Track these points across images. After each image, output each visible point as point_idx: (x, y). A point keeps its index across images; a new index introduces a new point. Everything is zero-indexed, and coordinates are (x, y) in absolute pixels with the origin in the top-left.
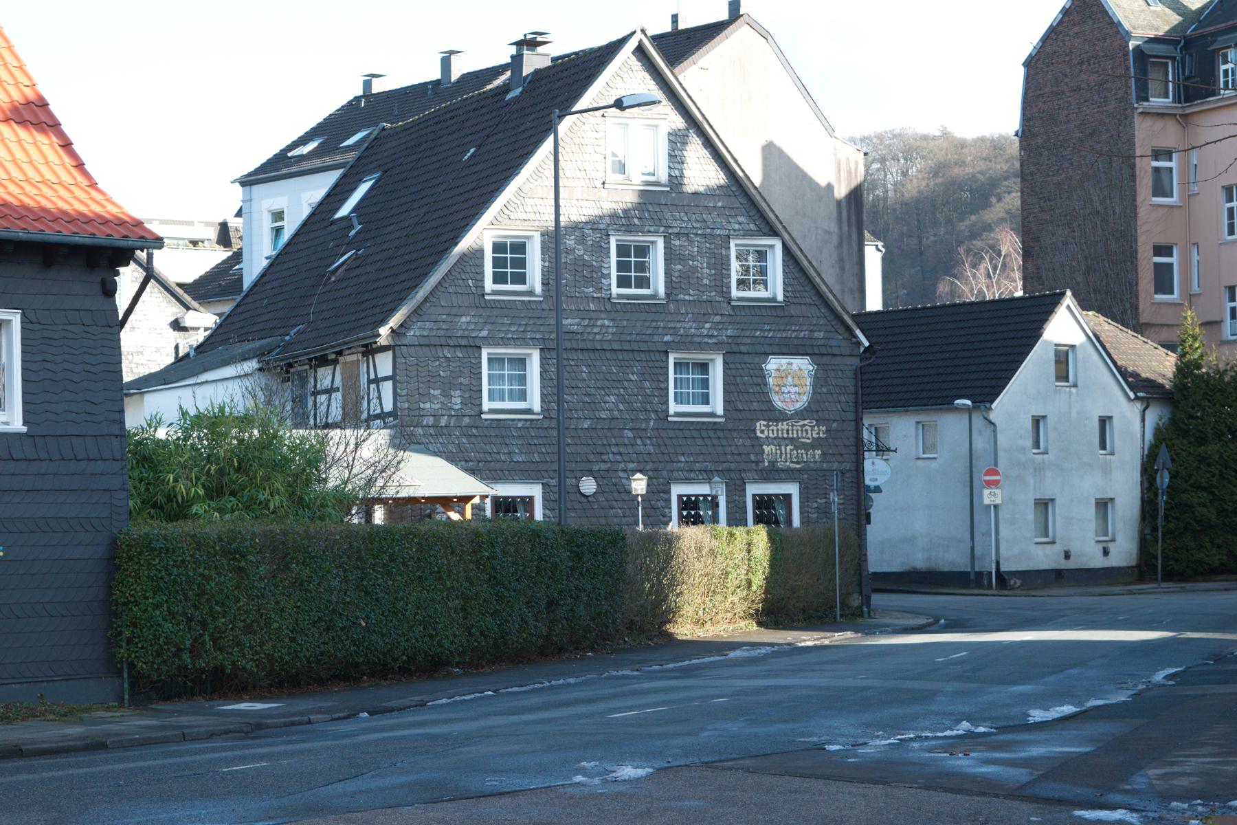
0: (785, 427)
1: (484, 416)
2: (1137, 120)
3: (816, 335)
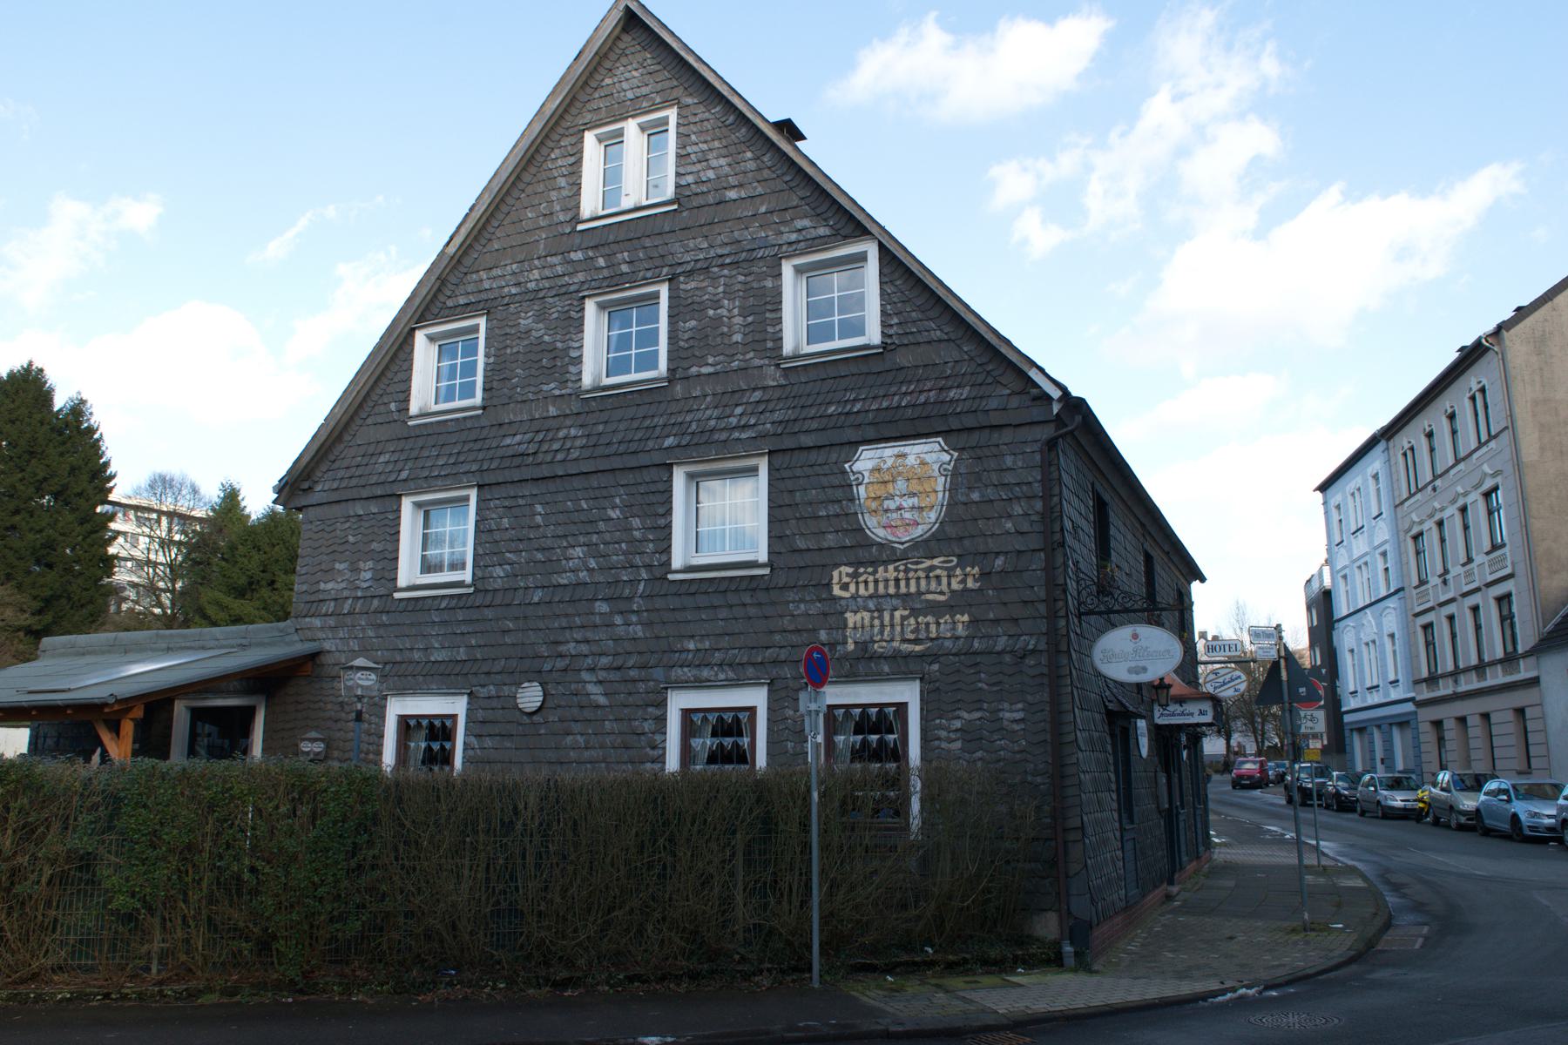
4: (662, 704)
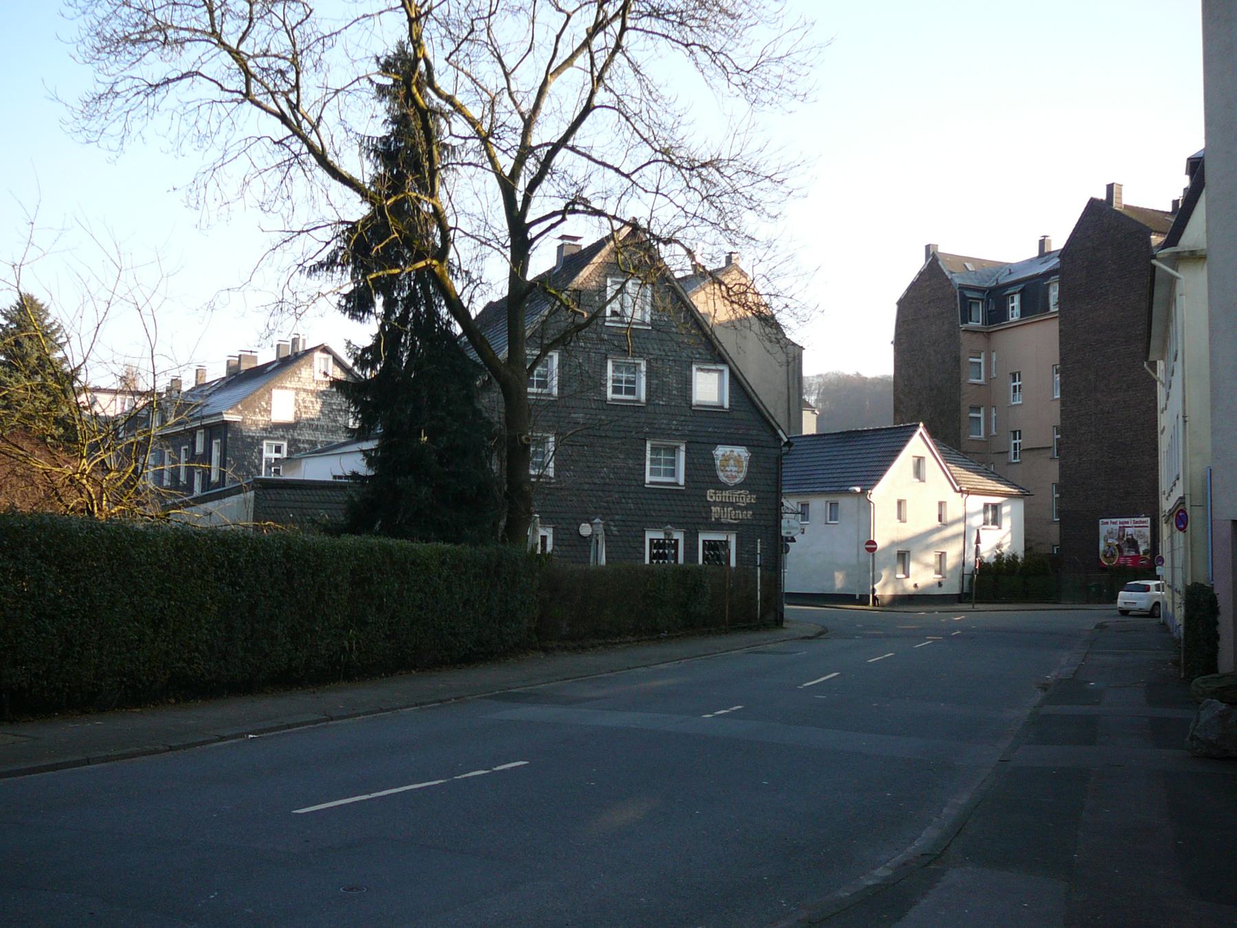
0: (728, 495)
2: (961, 334)
3: (751, 432)
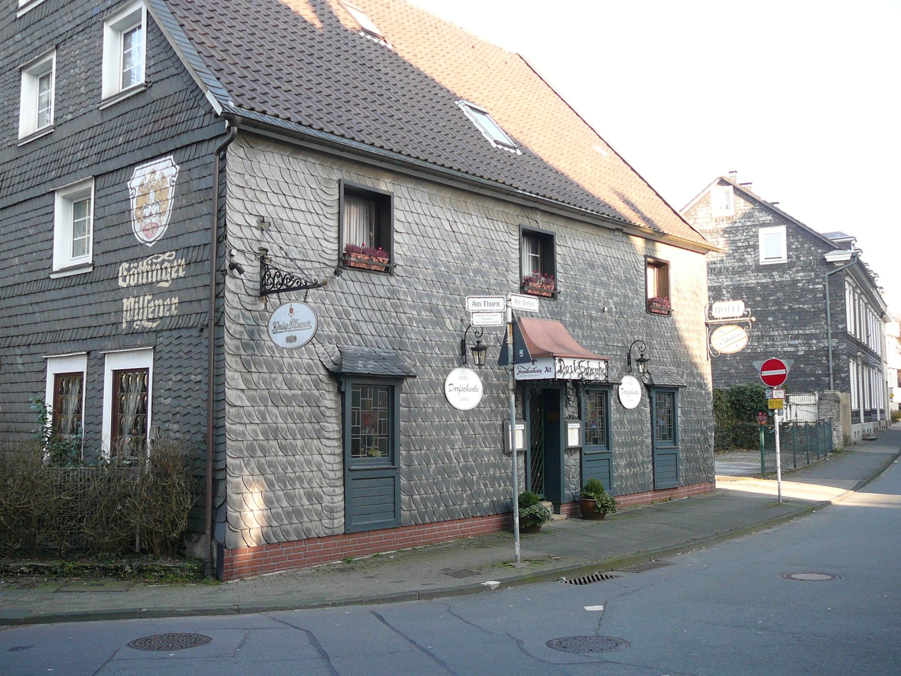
1: (53, 276)
4: (44, 371)
